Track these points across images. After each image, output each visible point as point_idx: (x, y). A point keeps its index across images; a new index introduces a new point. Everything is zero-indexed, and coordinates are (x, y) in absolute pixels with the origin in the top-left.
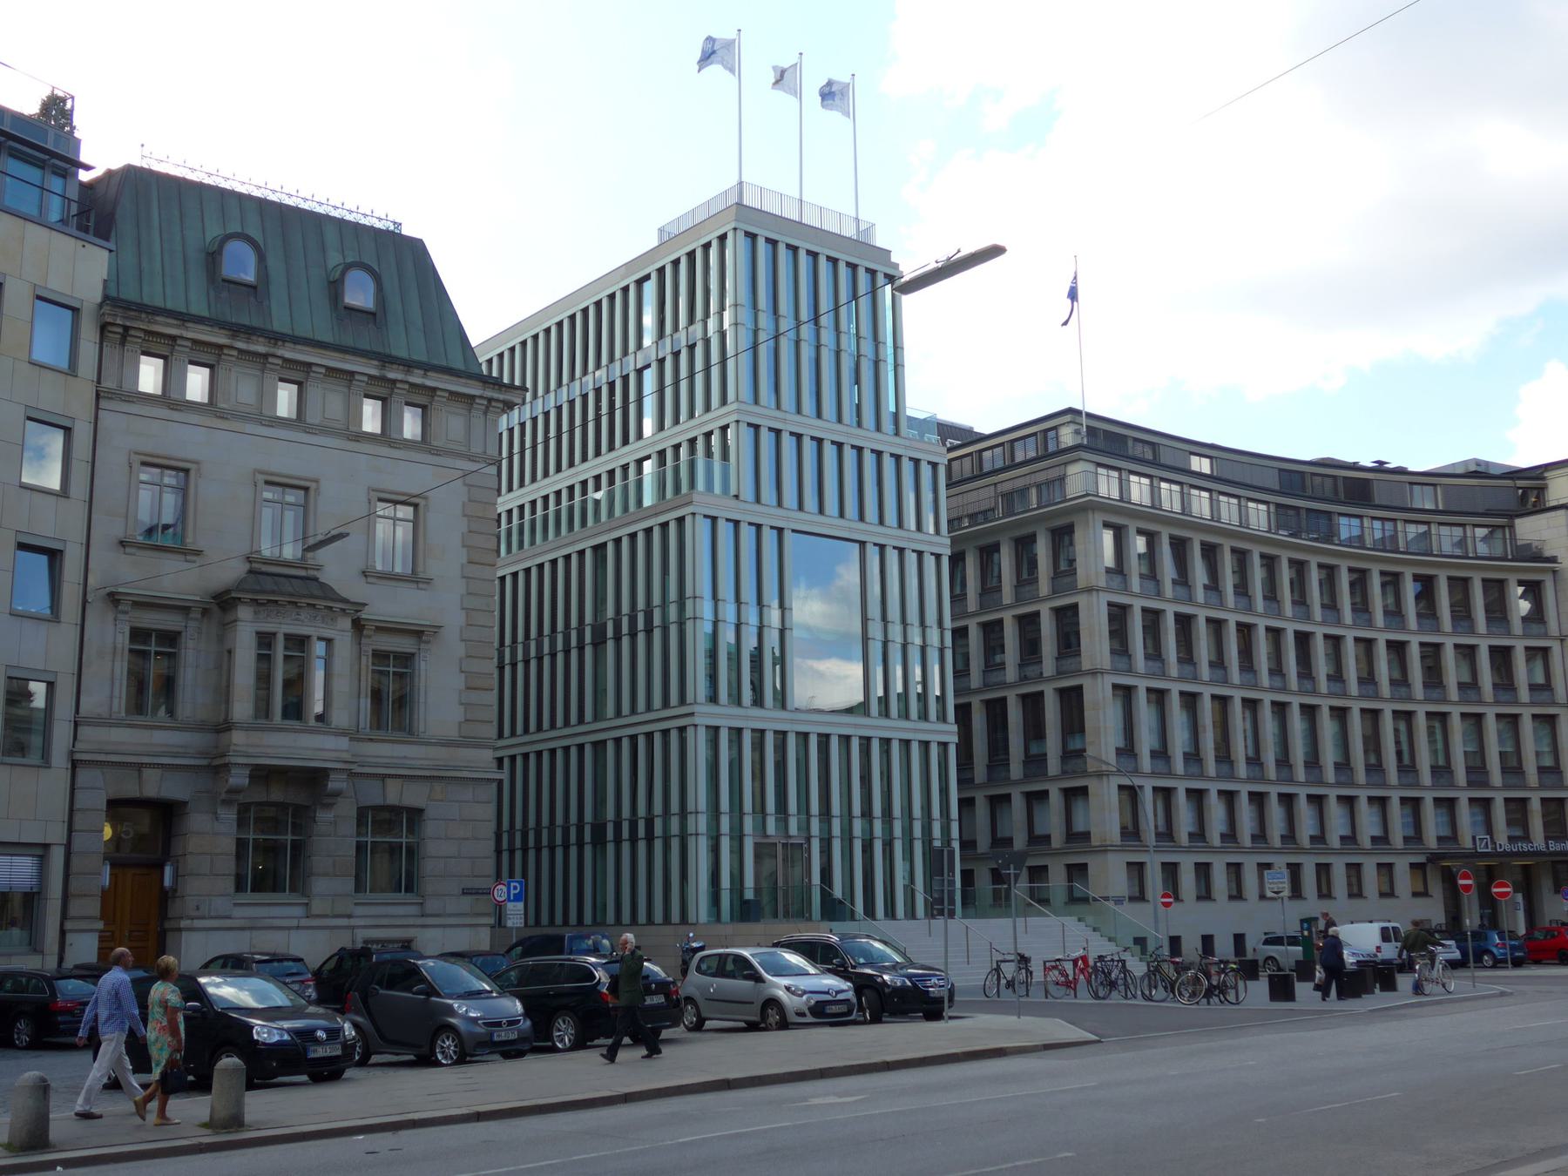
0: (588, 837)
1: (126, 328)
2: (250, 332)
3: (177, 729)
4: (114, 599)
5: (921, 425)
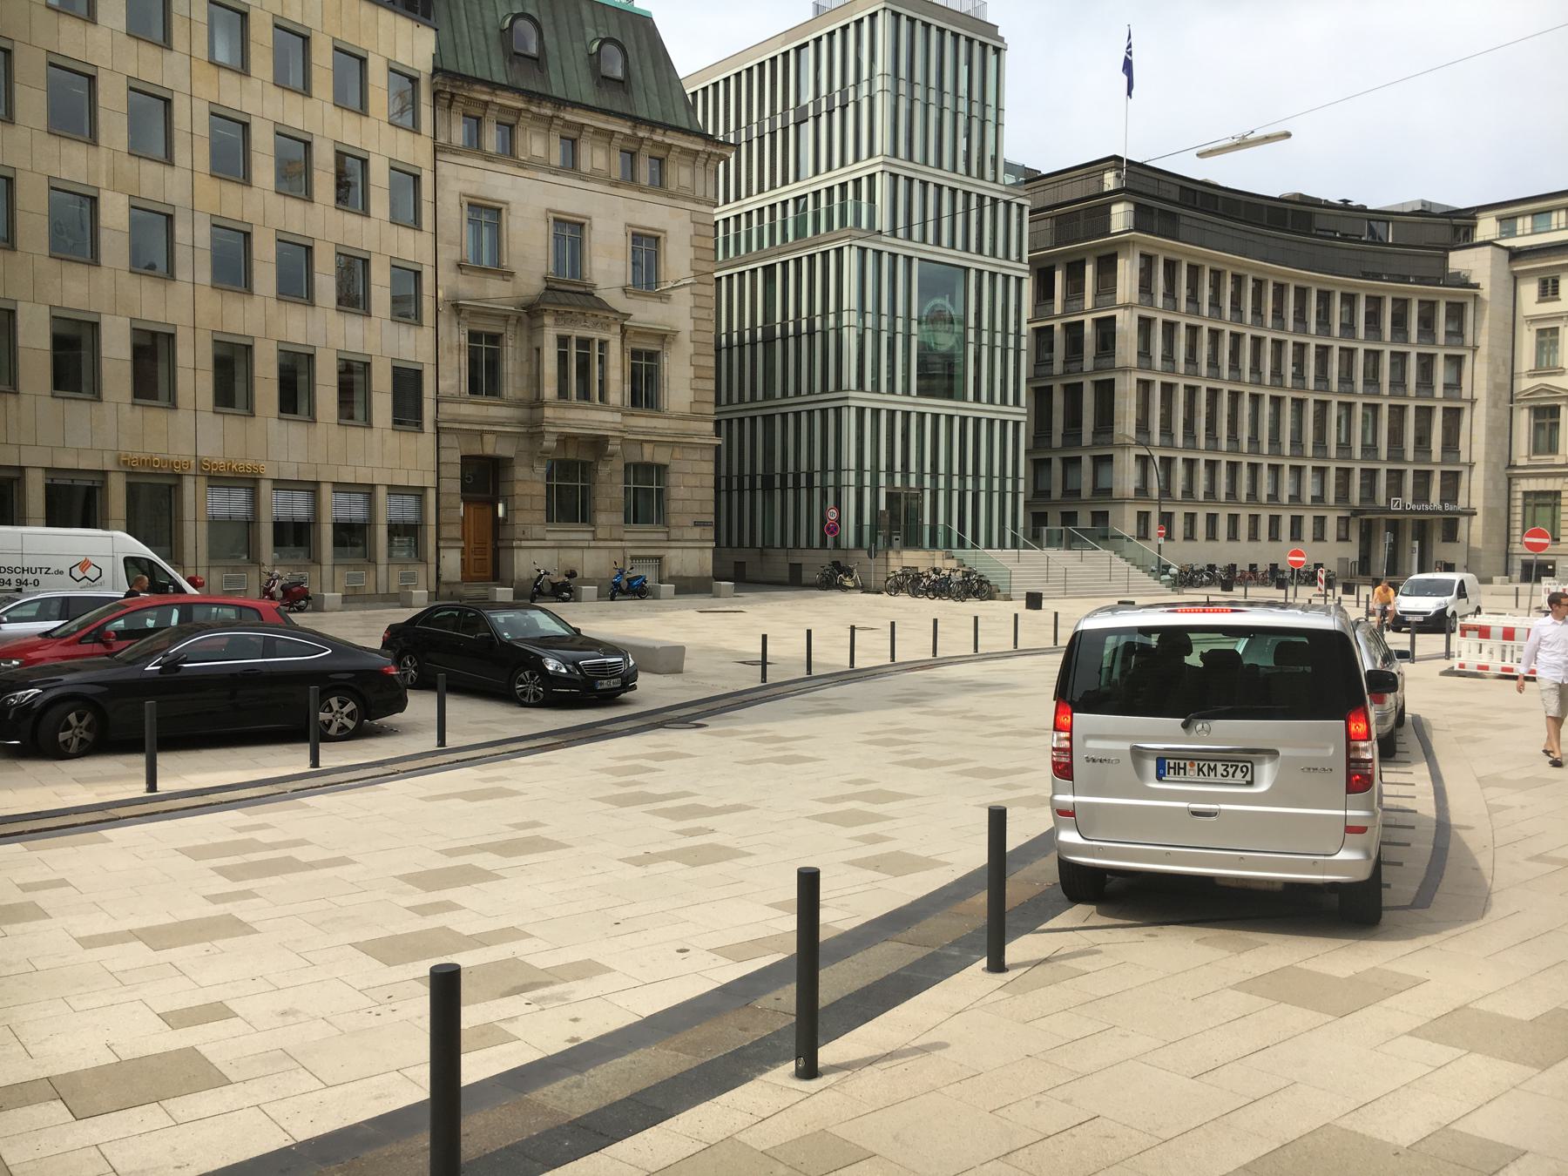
0: (759, 484)
1: (453, 95)
2: (541, 98)
3: (504, 405)
4: (457, 308)
5: (1011, 168)
